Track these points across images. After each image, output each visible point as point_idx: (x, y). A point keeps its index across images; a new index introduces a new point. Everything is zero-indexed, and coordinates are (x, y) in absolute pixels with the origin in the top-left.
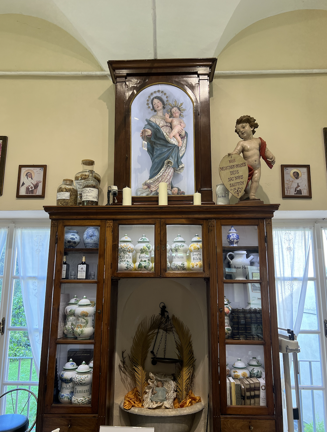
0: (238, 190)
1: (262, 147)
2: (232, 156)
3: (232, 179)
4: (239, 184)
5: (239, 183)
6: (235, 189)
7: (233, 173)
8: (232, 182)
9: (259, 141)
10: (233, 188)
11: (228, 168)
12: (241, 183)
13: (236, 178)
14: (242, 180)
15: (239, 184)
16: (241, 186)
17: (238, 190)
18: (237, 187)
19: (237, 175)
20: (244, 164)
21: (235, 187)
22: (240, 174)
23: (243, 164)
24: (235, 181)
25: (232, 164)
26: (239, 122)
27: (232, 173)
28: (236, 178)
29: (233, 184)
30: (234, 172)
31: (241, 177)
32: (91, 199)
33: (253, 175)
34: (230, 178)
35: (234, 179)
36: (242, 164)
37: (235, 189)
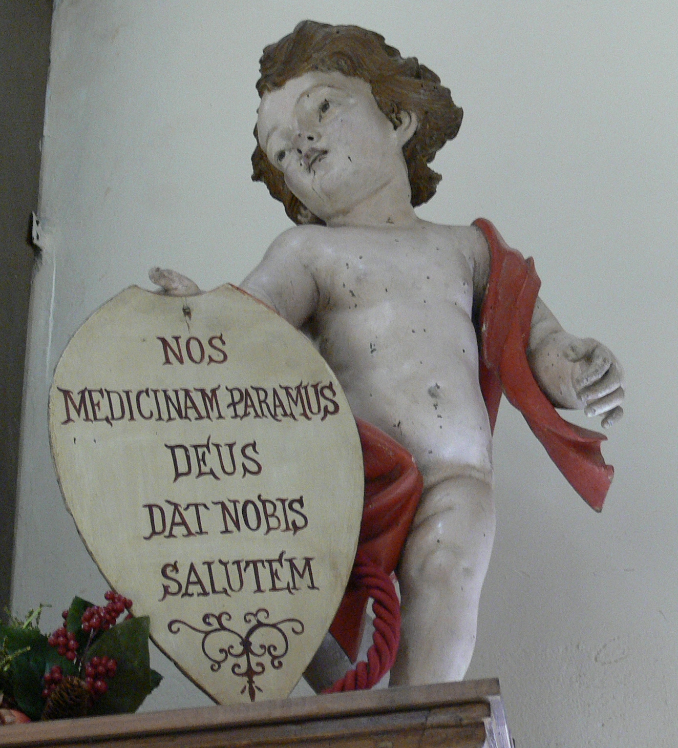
0: (246, 644)
1: (502, 297)
2: (198, 304)
3: (190, 516)
4: (266, 582)
5: (264, 573)
6: (216, 622)
7: (202, 460)
8: (185, 551)
9: (477, 246)
10: (193, 609)
11: (148, 404)
12: (285, 573)
13: (235, 516)
14: (294, 547)
15: (266, 582)
16: (279, 605)
17: (246, 644)
18: (239, 605)
19: (239, 488)
20: (319, 393)
21: (214, 604)
22: (276, 483)
23: (307, 400)
24: (214, 545)
25: (189, 376)
26: (280, 64)
27: (190, 460)
28: (235, 516)
29: (203, 571)
30: (212, 460)
31: (292, 512)
32: (6, 719)
33: (410, 530)
34: (169, 510)
35: (213, 519)
36: (299, 393)
37: (216, 622)
